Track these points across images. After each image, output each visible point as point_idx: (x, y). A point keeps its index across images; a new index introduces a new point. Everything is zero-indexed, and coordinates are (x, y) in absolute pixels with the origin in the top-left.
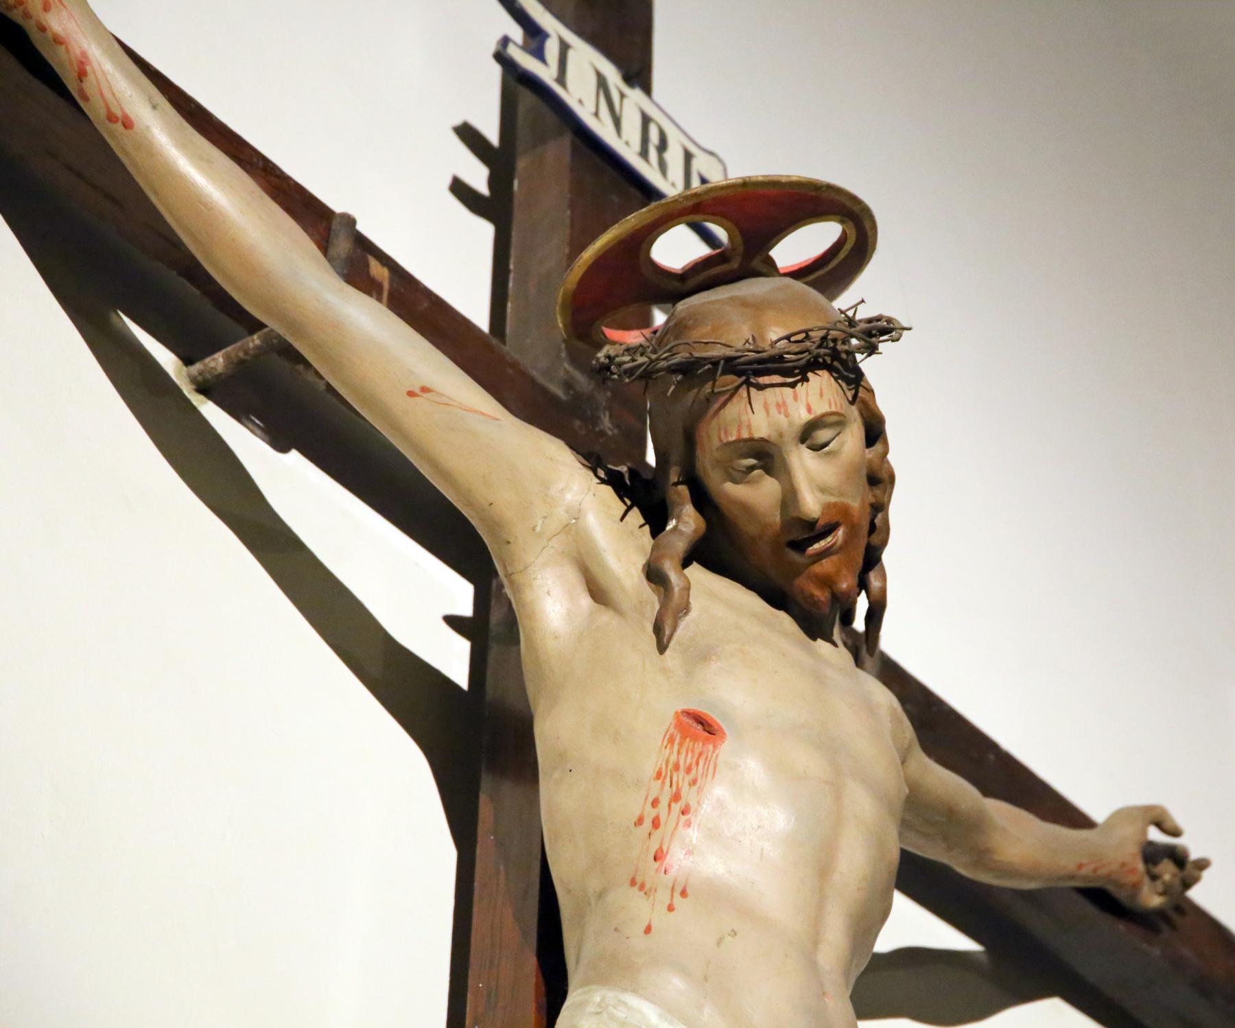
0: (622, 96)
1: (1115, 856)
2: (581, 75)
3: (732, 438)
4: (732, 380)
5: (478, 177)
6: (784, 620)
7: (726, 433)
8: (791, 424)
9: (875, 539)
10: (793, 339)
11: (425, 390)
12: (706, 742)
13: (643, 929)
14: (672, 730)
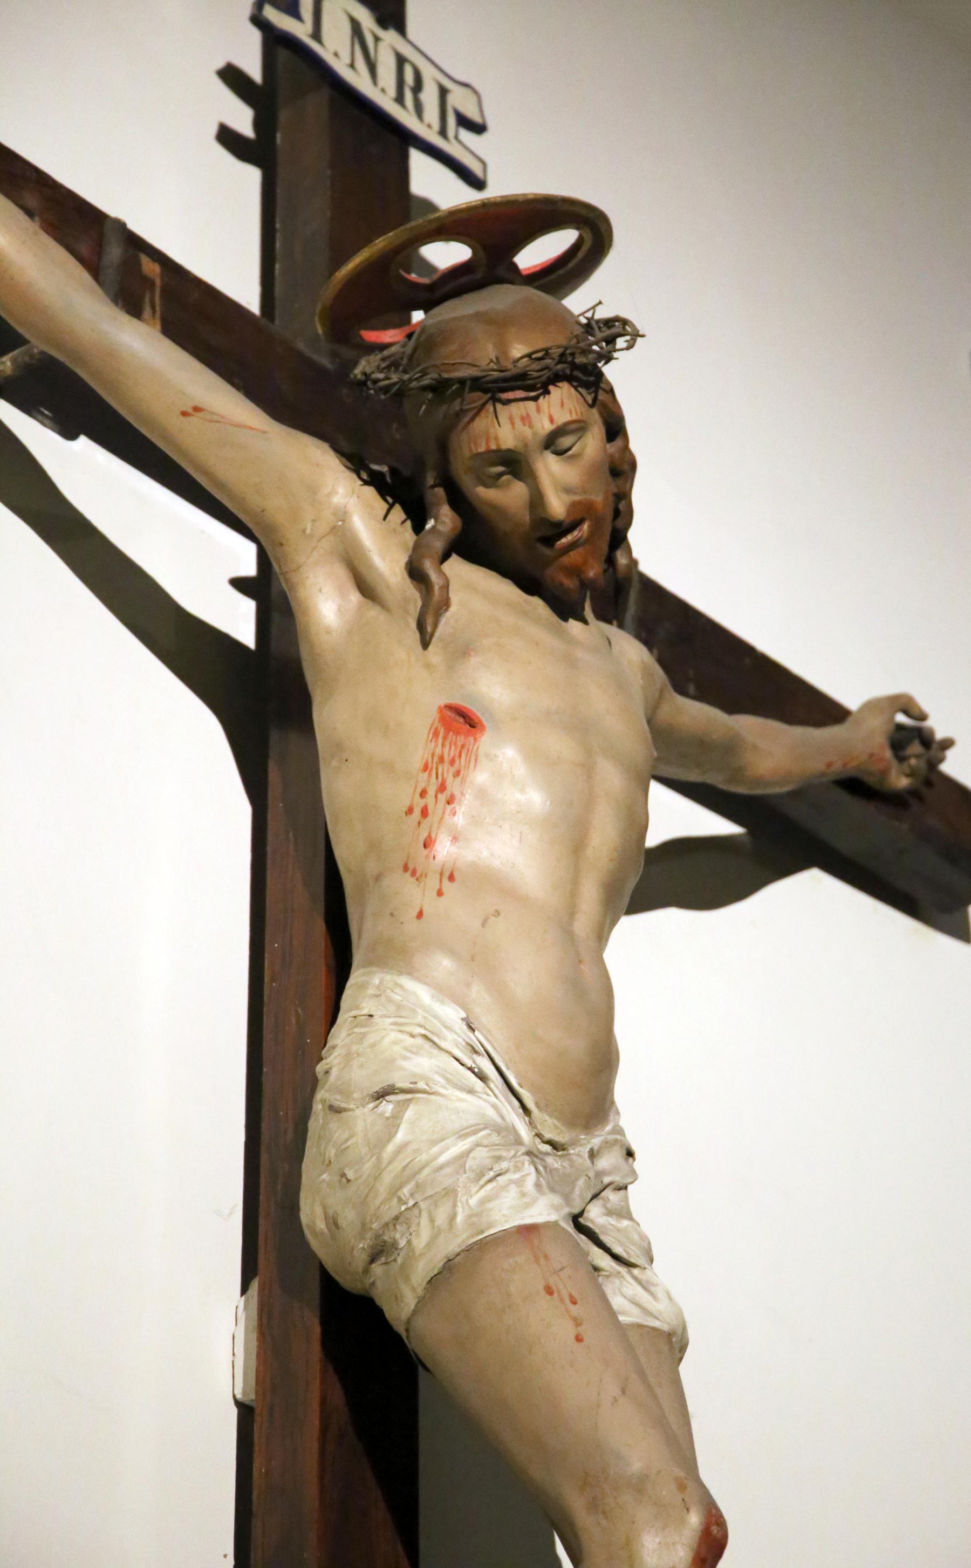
0: (377, 39)
1: (860, 745)
3: (482, 449)
4: (478, 397)
5: (242, 119)
6: (537, 604)
7: (476, 444)
8: (535, 434)
9: (620, 523)
10: (533, 356)
11: (197, 409)
12: (468, 734)
14: (436, 724)
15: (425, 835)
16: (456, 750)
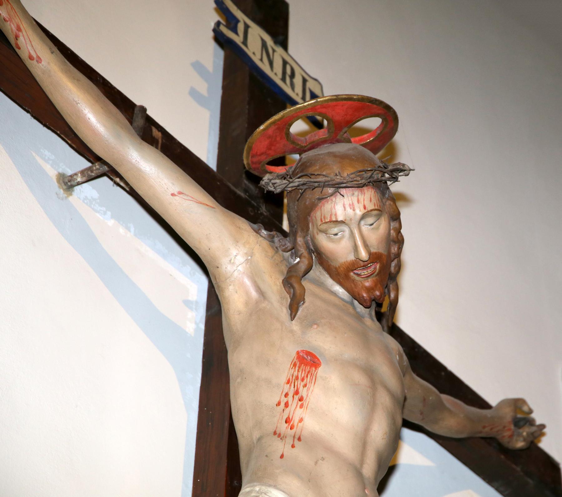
0: (274, 51)
2: (254, 39)
13: (280, 456)
14: (295, 360)
15: (287, 416)
16: (305, 373)
